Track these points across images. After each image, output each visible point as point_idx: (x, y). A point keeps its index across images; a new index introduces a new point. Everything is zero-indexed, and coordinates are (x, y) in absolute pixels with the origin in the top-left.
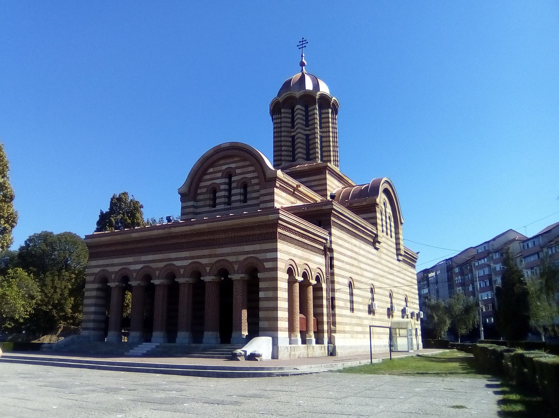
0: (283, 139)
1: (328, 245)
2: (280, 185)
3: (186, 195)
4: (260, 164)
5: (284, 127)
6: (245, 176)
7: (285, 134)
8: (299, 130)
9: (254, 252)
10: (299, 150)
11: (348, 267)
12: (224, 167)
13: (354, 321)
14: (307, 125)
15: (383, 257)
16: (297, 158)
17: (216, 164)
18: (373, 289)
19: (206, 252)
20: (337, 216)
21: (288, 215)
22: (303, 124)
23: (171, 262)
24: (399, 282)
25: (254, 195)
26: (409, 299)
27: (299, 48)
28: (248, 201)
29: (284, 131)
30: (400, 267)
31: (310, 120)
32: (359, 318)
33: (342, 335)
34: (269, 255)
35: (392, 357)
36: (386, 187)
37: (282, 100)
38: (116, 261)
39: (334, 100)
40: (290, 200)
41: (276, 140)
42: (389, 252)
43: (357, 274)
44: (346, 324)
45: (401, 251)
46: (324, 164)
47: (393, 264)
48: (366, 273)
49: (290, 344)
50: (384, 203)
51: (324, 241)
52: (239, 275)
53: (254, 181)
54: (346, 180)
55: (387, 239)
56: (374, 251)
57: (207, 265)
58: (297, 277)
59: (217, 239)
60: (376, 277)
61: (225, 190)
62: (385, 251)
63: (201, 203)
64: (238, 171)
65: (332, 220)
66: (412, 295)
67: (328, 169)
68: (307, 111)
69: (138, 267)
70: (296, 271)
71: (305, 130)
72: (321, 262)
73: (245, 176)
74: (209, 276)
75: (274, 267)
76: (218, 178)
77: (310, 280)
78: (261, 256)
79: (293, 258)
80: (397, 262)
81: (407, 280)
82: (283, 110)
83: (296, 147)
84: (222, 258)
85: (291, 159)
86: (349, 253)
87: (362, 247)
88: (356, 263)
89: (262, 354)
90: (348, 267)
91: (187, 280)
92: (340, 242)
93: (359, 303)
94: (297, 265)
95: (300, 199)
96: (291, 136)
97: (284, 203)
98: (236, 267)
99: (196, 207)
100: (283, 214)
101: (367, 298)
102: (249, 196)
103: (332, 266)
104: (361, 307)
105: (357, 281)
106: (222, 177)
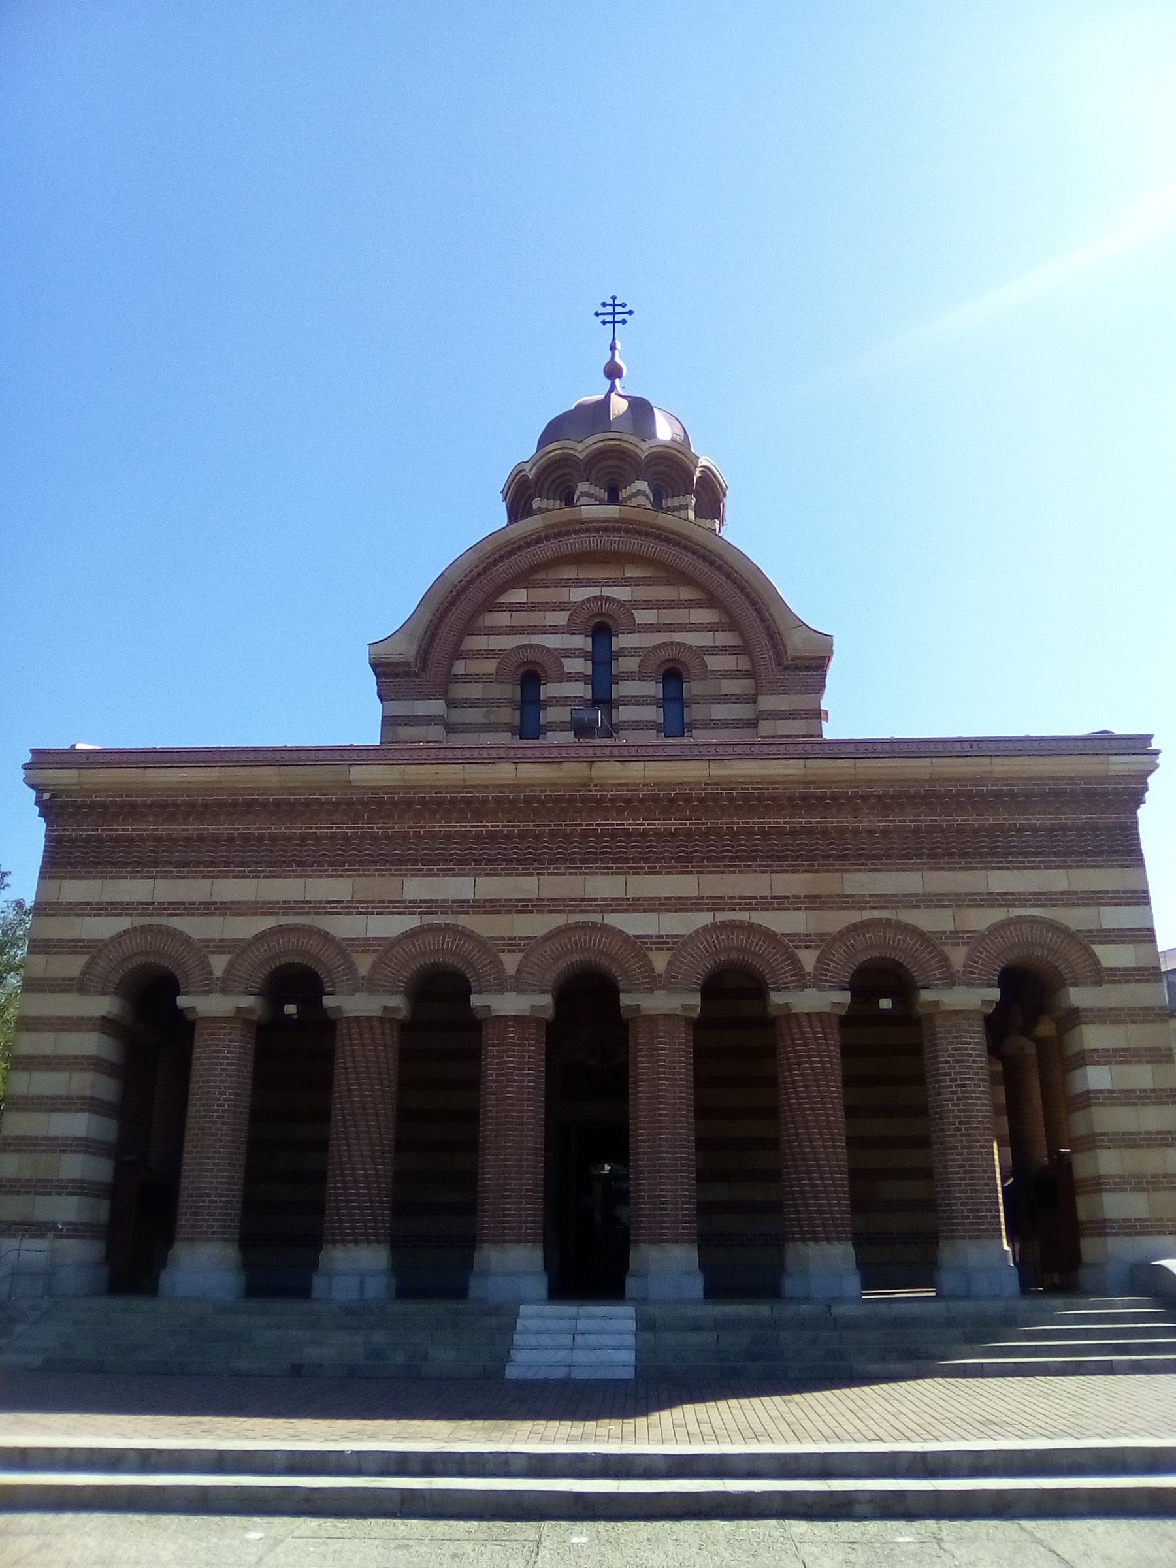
3: (407, 674)
4: (753, 603)
6: (677, 637)
12: (579, 595)
17: (541, 576)
23: (596, 918)
27: (604, 323)
34: (1114, 917)
57: (806, 941)
59: (842, 831)
63: (474, 715)
64: (643, 617)
74: (820, 988)
76: (553, 630)
78: (1075, 918)
84: (876, 914)
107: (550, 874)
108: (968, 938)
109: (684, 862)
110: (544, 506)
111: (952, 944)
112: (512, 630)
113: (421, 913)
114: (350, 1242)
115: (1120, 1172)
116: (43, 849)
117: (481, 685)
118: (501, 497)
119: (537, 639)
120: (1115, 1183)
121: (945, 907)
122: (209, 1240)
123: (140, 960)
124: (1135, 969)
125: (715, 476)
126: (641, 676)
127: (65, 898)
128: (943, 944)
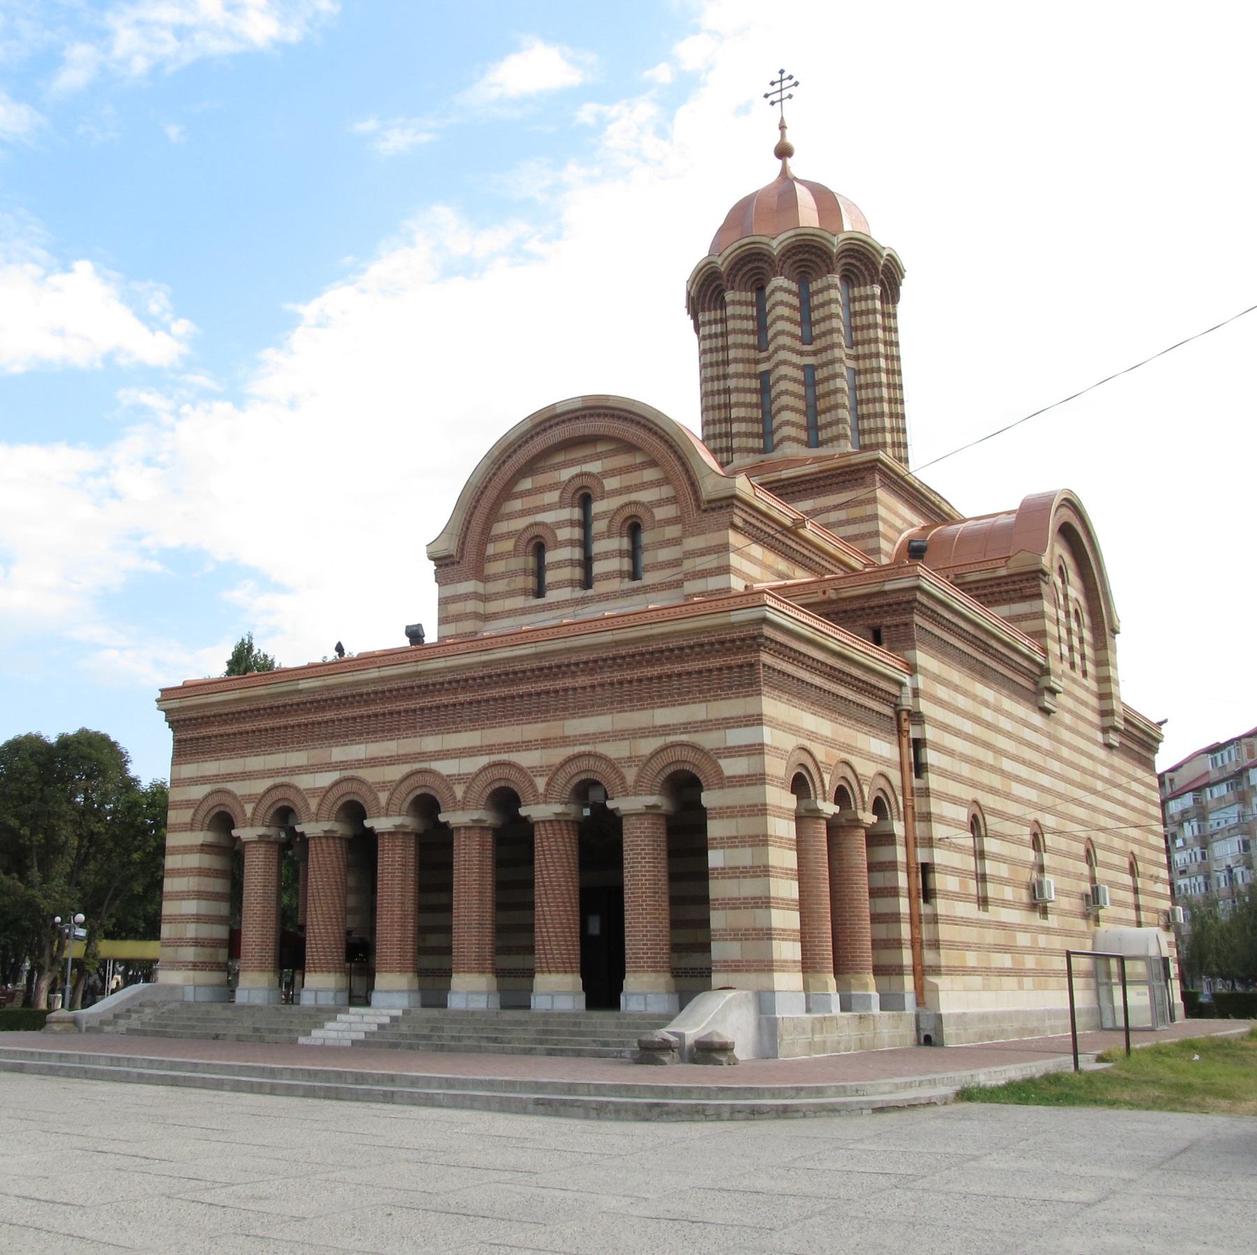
0: (732, 383)
1: (907, 702)
2: (744, 520)
4: (680, 458)
5: (736, 346)
6: (634, 497)
7: (740, 368)
8: (783, 355)
9: (687, 727)
10: (787, 415)
11: (966, 770)
12: (566, 474)
13: (991, 936)
15: (1063, 738)
16: (781, 441)
18: (1040, 836)
19: (533, 731)
20: (932, 611)
21: (791, 608)
22: (793, 336)
24: (1110, 815)
25: (664, 555)
26: (1141, 866)
27: (773, 103)
28: (548, 594)
29: (736, 361)
30: (1112, 767)
31: (818, 322)
32: (1003, 926)
33: (959, 981)
35: (1132, 1046)
36: (1067, 520)
37: (727, 262)
38: (255, 763)
39: (888, 255)
40: (776, 567)
41: (709, 389)
42: (1079, 722)
43: (993, 791)
44: (967, 946)
45: (1116, 718)
46: (868, 456)
47: (1090, 757)
48: (1018, 789)
49: (808, 1010)
50: (1060, 568)
51: (893, 689)
52: (640, 798)
53: (661, 513)
54: (933, 503)
55: (1074, 681)
56: (1037, 719)
58: (821, 804)
60: (1049, 800)
61: (571, 543)
62: (1067, 719)
64: (611, 484)
65: (916, 625)
66: (1149, 854)
67: (880, 471)
68: (805, 297)
69: (325, 779)
70: (818, 783)
71: (801, 354)
72: (889, 757)
73: (634, 497)
75: (752, 772)
77: (859, 811)
78: (708, 740)
79: (807, 744)
80: (1102, 753)
81: (1134, 809)
82: (729, 296)
83: (774, 408)
86: (968, 727)
87: (1004, 707)
88: (988, 757)
89: (734, 1043)
90: (966, 770)
91: (475, 818)
92: (942, 692)
93: (1003, 881)
94: (820, 765)
95: (805, 564)
96: (758, 372)
97: (759, 577)
98: (630, 774)
99: (485, 598)
100: (776, 606)
101: (1023, 864)
102: (646, 558)
103: (920, 768)
104: (1008, 893)
105: (995, 813)
106: (561, 504)
107: (404, 738)
108: (639, 761)
109: (475, 723)
111: (629, 766)
113: (341, 770)
114: (553, 972)
116: (172, 747)
120: (720, 935)
121: (625, 739)
122: (252, 971)
125: (865, 242)
126: (609, 534)
128: (622, 767)
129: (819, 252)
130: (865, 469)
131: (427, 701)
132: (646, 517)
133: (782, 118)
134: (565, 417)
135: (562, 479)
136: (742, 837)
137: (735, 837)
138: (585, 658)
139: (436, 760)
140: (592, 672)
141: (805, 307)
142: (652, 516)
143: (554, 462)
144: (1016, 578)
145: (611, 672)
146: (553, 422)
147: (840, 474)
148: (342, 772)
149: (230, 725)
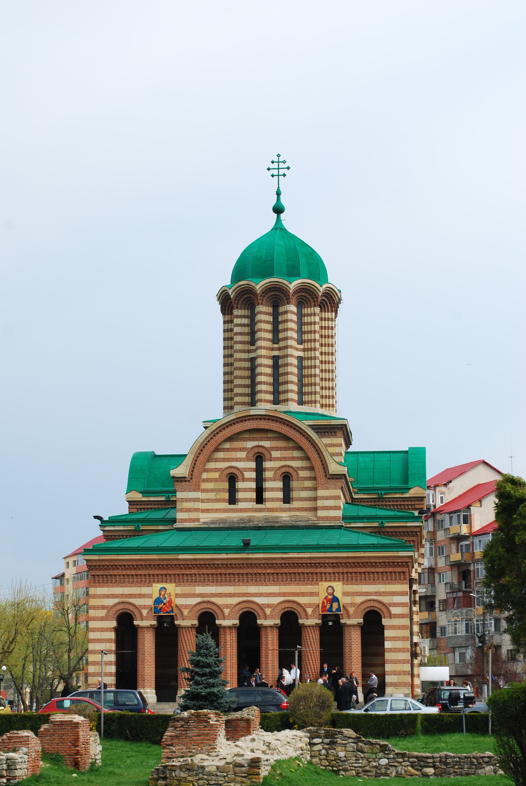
9: (376, 593)
10: (263, 387)
14: (276, 340)
27: (273, 176)
64: (275, 454)
68: (276, 315)
71: (272, 349)
78: (385, 599)
85: (247, 399)
86: (196, 505)
106: (247, 459)
107: (237, 586)
109: (275, 583)
110: (240, 314)
112: (224, 460)
115: (391, 670)
117: (213, 483)
118: (216, 298)
119: (234, 464)
121: (349, 596)
123: (122, 611)
124: (401, 614)
126: (274, 479)
127: (98, 593)
129: (311, 293)
130: (337, 428)
131: (250, 571)
132: (294, 474)
133: (278, 187)
134: (254, 417)
135: (248, 447)
136: (399, 637)
137: (396, 637)
138: (332, 561)
139: (255, 597)
140: (334, 567)
141: (276, 323)
142: (298, 474)
143: (244, 437)
144: (413, 499)
145: (343, 568)
146: (246, 418)
147: (323, 428)
148: (202, 598)
149: (129, 570)
